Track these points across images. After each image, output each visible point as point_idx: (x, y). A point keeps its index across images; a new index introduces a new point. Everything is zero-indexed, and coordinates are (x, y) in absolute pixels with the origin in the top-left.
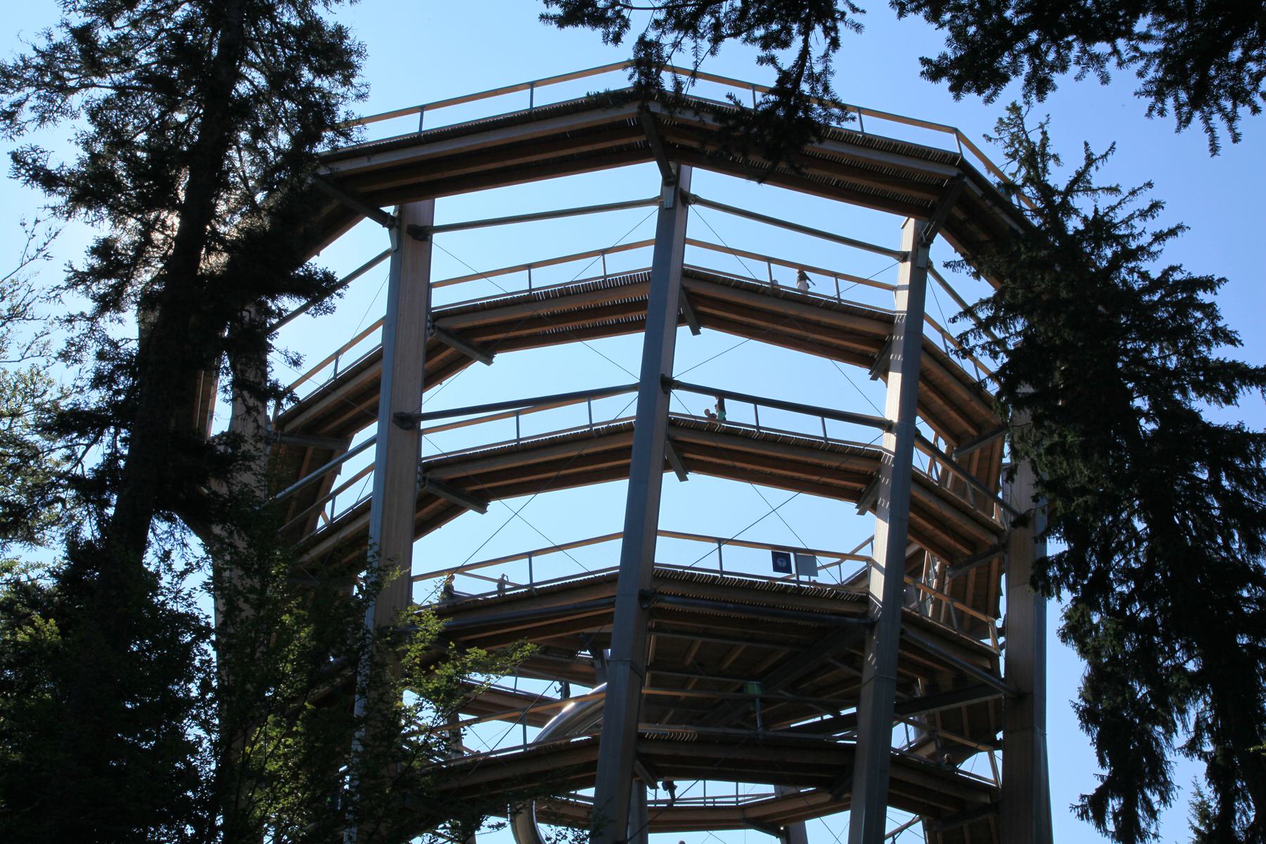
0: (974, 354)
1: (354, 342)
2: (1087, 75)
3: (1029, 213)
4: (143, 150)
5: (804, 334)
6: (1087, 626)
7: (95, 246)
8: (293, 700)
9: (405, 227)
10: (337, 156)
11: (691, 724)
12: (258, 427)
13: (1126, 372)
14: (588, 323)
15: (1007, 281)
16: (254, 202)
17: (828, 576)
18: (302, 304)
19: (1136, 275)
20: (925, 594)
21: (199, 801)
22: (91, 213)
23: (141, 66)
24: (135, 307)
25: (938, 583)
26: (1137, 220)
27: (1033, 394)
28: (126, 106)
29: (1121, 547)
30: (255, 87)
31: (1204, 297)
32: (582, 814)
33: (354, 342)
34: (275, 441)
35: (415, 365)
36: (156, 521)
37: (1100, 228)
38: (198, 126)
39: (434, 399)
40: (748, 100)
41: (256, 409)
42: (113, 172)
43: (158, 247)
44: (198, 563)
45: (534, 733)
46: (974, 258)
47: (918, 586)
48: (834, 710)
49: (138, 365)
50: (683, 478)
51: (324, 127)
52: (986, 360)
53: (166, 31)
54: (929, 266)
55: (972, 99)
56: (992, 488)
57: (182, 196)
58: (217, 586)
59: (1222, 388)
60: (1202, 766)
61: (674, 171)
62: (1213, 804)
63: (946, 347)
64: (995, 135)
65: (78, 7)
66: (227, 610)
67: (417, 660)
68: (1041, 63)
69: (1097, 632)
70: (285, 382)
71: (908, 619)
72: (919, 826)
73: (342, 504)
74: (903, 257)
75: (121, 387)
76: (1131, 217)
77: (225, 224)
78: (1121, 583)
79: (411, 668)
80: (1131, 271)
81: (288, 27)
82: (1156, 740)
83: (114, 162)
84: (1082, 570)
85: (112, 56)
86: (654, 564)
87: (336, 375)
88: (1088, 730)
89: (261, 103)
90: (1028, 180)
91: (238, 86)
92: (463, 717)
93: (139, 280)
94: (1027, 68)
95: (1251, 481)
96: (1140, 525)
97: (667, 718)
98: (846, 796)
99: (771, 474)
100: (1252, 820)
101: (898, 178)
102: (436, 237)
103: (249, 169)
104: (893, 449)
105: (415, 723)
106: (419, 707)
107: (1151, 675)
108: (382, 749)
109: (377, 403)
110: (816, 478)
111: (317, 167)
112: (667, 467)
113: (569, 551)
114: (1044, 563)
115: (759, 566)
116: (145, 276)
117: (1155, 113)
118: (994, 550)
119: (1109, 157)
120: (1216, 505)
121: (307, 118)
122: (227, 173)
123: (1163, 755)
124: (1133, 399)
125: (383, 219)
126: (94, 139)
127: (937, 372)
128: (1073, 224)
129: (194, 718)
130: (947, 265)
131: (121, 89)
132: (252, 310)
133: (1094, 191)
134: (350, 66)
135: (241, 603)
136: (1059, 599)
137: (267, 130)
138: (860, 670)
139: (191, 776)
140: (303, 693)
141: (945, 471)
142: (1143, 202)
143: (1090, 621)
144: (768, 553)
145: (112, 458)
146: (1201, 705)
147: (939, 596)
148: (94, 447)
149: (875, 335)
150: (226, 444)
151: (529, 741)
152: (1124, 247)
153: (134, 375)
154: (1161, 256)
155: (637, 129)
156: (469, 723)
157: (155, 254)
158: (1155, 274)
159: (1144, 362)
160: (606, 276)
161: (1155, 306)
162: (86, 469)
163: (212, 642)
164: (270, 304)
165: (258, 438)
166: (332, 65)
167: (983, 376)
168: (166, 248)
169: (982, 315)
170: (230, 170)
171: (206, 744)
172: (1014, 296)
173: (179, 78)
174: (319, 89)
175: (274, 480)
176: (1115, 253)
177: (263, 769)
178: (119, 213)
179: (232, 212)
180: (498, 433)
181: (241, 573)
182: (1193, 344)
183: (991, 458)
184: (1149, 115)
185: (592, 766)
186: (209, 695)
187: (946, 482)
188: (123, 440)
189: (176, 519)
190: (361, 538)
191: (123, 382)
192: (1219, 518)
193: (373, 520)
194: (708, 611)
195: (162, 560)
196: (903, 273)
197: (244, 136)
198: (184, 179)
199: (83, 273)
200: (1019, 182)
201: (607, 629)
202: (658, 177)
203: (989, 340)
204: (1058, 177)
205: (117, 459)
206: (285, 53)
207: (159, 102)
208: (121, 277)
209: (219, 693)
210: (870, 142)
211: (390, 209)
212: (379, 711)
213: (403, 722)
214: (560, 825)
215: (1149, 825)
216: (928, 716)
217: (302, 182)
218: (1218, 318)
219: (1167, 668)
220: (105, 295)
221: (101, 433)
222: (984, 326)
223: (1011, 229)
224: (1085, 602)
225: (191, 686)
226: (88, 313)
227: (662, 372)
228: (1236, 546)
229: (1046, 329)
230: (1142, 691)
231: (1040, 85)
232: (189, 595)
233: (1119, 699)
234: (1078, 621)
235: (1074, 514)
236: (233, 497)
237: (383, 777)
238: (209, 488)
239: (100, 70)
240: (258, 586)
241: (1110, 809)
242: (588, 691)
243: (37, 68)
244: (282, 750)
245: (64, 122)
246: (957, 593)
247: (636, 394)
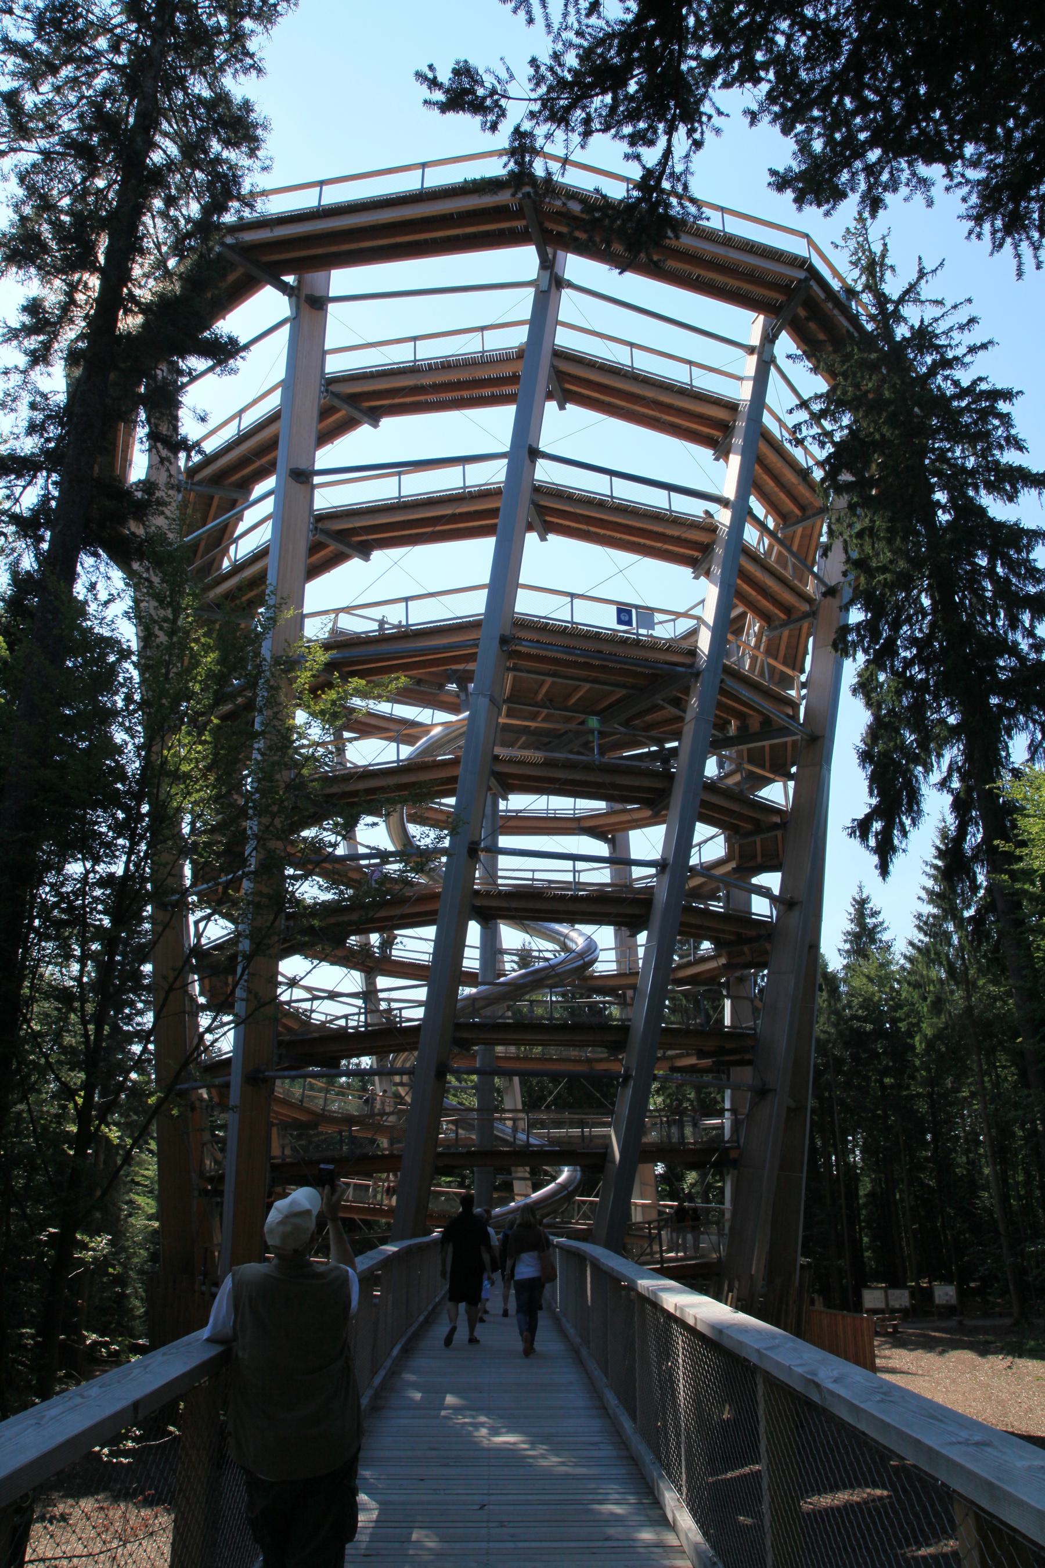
0: (806, 443)
1: (255, 402)
2: (915, 197)
3: (864, 318)
4: (67, 214)
6: (874, 683)
7: (25, 304)
8: (202, 714)
9: (303, 296)
10: (242, 226)
11: (537, 748)
12: (171, 476)
13: (931, 468)
14: (466, 394)
15: (840, 379)
16: (166, 267)
17: (665, 631)
19: (949, 382)
20: (744, 650)
21: (126, 793)
22: (21, 272)
23: (64, 132)
24: (63, 362)
25: (756, 641)
26: (956, 332)
27: (852, 482)
28: (51, 170)
29: (909, 620)
30: (168, 156)
31: (1003, 406)
32: (443, 817)
33: (255, 402)
34: (186, 489)
35: (311, 425)
36: (84, 556)
37: (923, 338)
38: (117, 193)
39: (326, 457)
40: (616, 191)
41: (168, 460)
42: (39, 234)
43: (81, 307)
44: (119, 594)
45: (406, 751)
46: (814, 355)
47: (739, 642)
48: (660, 742)
49: (66, 415)
50: (543, 539)
51: (231, 197)
52: (814, 449)
53: (87, 98)
54: (773, 360)
55: (813, 212)
56: (809, 563)
57: (102, 259)
58: (138, 615)
59: (1008, 488)
60: (950, 798)
61: (550, 256)
62: (952, 828)
63: (782, 436)
64: (842, 243)
65: (6, 71)
66: (146, 638)
67: (307, 686)
68: (875, 183)
69: (881, 688)
70: (193, 437)
71: (729, 671)
72: (721, 839)
73: (243, 548)
74: (751, 350)
75: (51, 435)
76: (951, 329)
77: (140, 287)
78: (906, 649)
79: (301, 692)
80: (946, 378)
81: (199, 98)
82: (916, 777)
83: (40, 225)
84: (875, 635)
85: (38, 121)
86: (514, 613)
87: (239, 431)
88: (864, 767)
89: (173, 172)
90: (867, 287)
91: (152, 155)
92: (347, 735)
93: (65, 337)
94: (863, 186)
95: (1020, 569)
96: (926, 602)
97: (519, 743)
98: (663, 813)
99: (620, 539)
100: (979, 840)
101: (752, 276)
102: (331, 307)
103: (162, 236)
104: (728, 523)
105: (305, 738)
106: (308, 724)
107: (919, 724)
108: (276, 758)
109: (275, 459)
110: (659, 545)
111: (224, 236)
112: (530, 528)
113: (440, 598)
114: (845, 629)
115: (605, 619)
116: (69, 334)
117: (973, 236)
118: (805, 616)
119: (938, 272)
120: (990, 588)
121: (216, 187)
122: (141, 239)
123: (919, 789)
124: (934, 492)
125: (284, 288)
126: (24, 203)
127: (772, 457)
128: (902, 332)
129: (122, 724)
130: (789, 357)
131: (46, 154)
132: (165, 369)
133: (922, 302)
134: (256, 139)
135: (156, 630)
136: (854, 660)
137: (179, 198)
138: (685, 711)
139: (120, 773)
140: (211, 708)
141: (771, 546)
142: (962, 316)
143: (877, 679)
144: (613, 609)
145: (46, 498)
146: (955, 750)
147: (756, 652)
148: (29, 488)
149: (722, 420)
150: (143, 491)
151: (402, 757)
152: (942, 355)
153: (62, 425)
154: (972, 367)
155: (519, 214)
156: (350, 740)
157: (78, 313)
158: (965, 383)
159: (947, 461)
160: (484, 352)
161: (961, 411)
162: (23, 508)
163: (133, 662)
164: (181, 364)
165: (170, 486)
166: (239, 138)
167: (811, 463)
168: (88, 308)
169: (816, 407)
170: (144, 235)
171: (130, 747)
172: (845, 393)
173: (99, 145)
174: (227, 161)
175: (186, 525)
176: (934, 361)
177: (178, 769)
178: (47, 273)
179: (146, 276)
181: (156, 604)
182: (988, 449)
183: (811, 535)
184: (968, 238)
185: (454, 779)
186: (132, 707)
187: (771, 555)
188: (54, 483)
189: (100, 555)
190: (260, 579)
191: (53, 431)
192: (990, 599)
193: (271, 562)
194: (559, 655)
195: (89, 590)
196: (749, 365)
197: (158, 203)
198: (103, 243)
199: (15, 329)
200: (859, 288)
201: (471, 666)
202: (536, 261)
203: (819, 431)
204: (893, 287)
205: (49, 500)
206: (196, 124)
207: (81, 168)
208: (49, 333)
209: (141, 706)
210: (729, 241)
211: (290, 279)
212: (274, 726)
213: (295, 736)
214: (424, 825)
215: (901, 842)
216: (737, 752)
217: (210, 250)
218: (1012, 426)
219: (932, 721)
220: (35, 351)
221: (35, 476)
222: (816, 418)
223: (848, 331)
224: (877, 661)
225: (116, 698)
226: (22, 367)
228: (1000, 623)
229: (868, 425)
230: (910, 737)
231: (874, 204)
232: (113, 622)
233: (891, 744)
234: (867, 679)
235: (875, 589)
236: (150, 539)
237: (277, 781)
238: (129, 529)
240: (171, 616)
241: (874, 830)
242: (453, 718)
244: (193, 755)
246: (771, 651)
247: (506, 461)
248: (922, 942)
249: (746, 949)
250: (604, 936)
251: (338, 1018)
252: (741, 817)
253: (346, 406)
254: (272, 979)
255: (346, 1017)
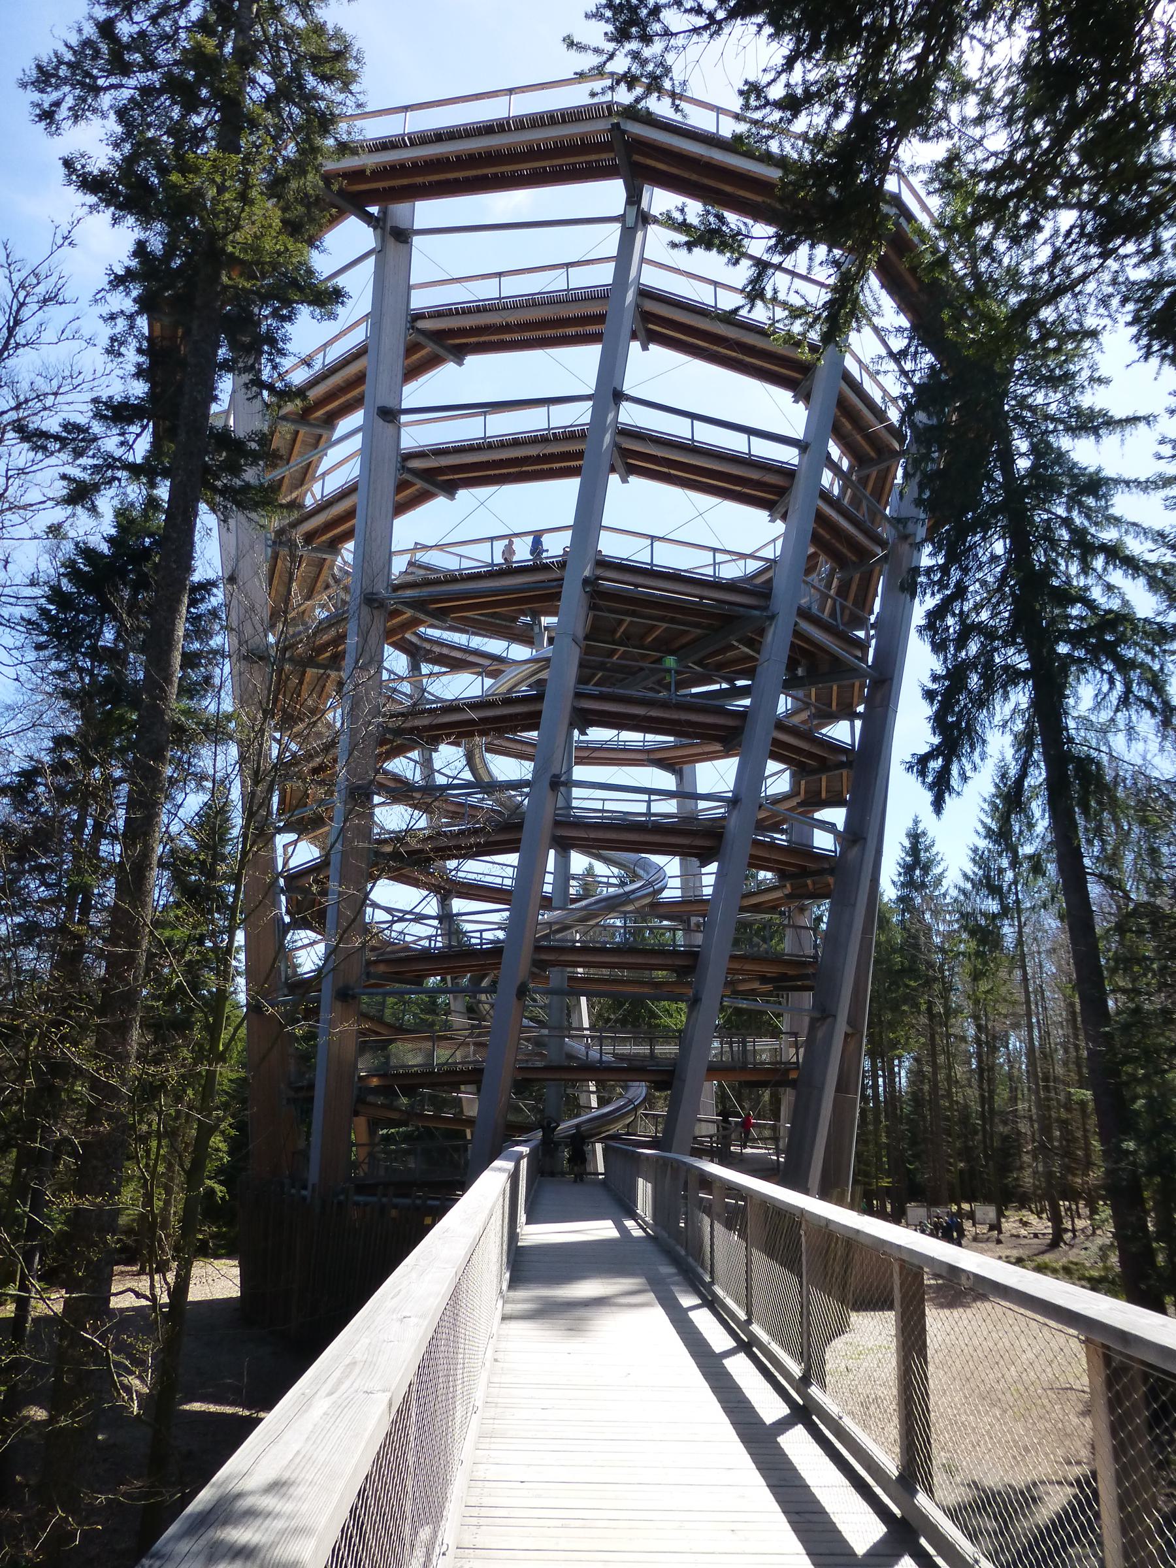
5: (740, 356)
14: (549, 333)
18: (1097, 919)
39: (416, 393)
73: (333, 483)
102: (416, 240)
112: (613, 469)
125: (368, 219)
131: (146, 91)
180: (468, 430)
211: (374, 210)
227: (614, 385)
239: (125, 69)
243: (69, 65)
245: (96, 121)
247: (591, 403)
248: (976, 875)
249: (809, 882)
250: (671, 865)
251: (421, 939)
252: (811, 755)
253: (431, 344)
254: (363, 900)
255: (429, 938)
